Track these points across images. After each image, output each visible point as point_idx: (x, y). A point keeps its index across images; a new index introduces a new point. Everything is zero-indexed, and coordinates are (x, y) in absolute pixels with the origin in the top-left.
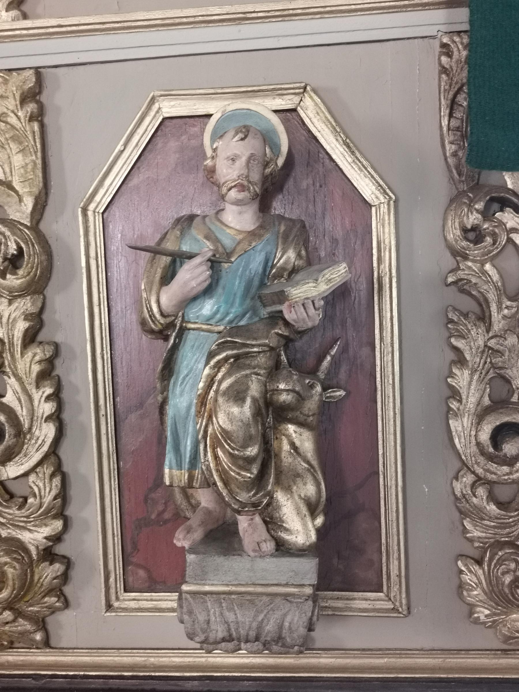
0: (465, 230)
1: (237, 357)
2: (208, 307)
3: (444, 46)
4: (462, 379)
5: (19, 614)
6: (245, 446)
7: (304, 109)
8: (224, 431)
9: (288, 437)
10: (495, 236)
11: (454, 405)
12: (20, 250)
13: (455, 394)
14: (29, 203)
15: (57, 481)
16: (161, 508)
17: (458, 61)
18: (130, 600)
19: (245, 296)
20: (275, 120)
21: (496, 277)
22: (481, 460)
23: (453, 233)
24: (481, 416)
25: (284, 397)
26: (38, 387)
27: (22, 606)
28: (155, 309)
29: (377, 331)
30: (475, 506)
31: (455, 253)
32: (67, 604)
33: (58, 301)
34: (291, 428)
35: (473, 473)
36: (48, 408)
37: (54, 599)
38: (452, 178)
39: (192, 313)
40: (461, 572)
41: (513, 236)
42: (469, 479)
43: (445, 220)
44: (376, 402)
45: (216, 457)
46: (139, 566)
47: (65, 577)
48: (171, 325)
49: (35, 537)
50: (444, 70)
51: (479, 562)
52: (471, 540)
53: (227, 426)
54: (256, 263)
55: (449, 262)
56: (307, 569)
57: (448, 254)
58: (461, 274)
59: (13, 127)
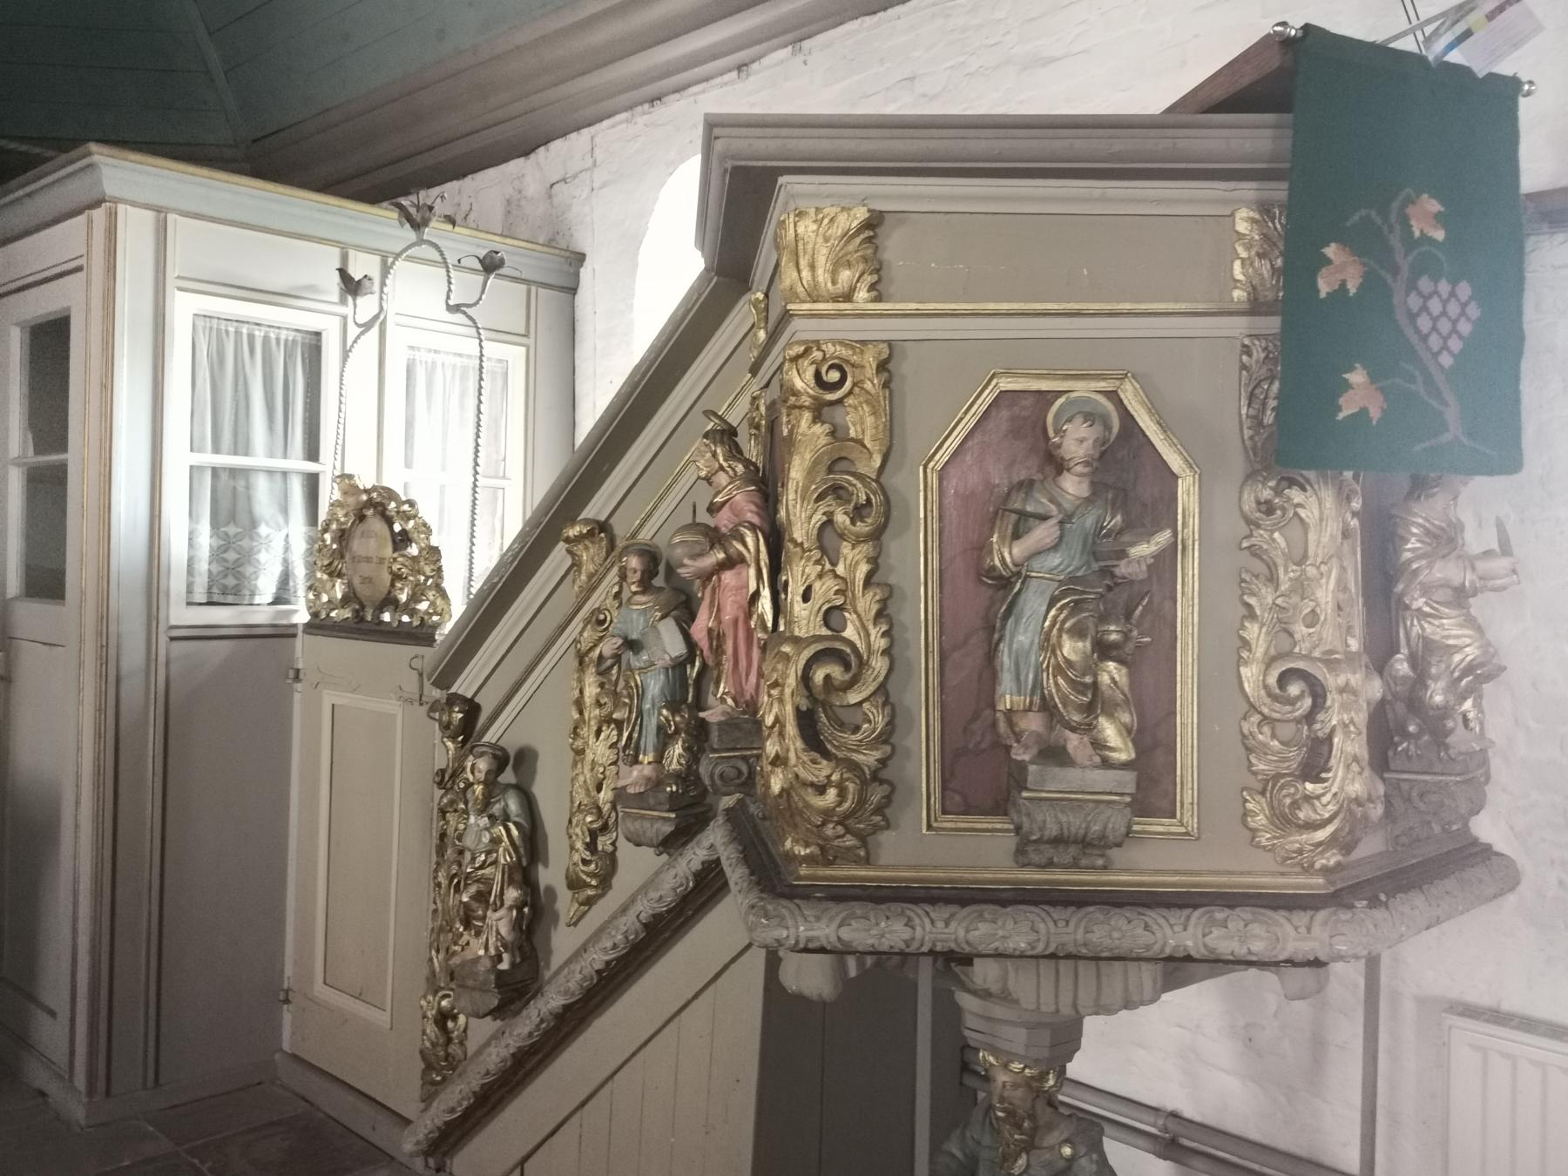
0: (1259, 503)
1: (1076, 602)
2: (1055, 560)
3: (1244, 346)
4: (1252, 631)
5: (848, 831)
6: (1084, 675)
7: (1124, 391)
8: (1067, 661)
9: (1109, 672)
10: (1284, 509)
11: (1245, 654)
12: (868, 500)
13: (1246, 644)
14: (877, 461)
15: (888, 710)
16: (978, 738)
17: (1257, 361)
18: (948, 822)
19: (1082, 553)
20: (1101, 399)
21: (1283, 545)
22: (1268, 701)
23: (1249, 504)
24: (1270, 662)
25: (1114, 637)
26: (875, 624)
27: (850, 822)
28: (1008, 560)
29: (1179, 587)
30: (1261, 743)
31: (1252, 523)
32: (888, 827)
33: (894, 546)
34: (1111, 665)
35: (1260, 713)
36: (881, 643)
37: (879, 818)
38: (1248, 457)
39: (1036, 564)
40: (1246, 801)
41: (1299, 510)
42: (1256, 718)
43: (1241, 493)
44: (1175, 649)
45: (1056, 684)
46: (954, 791)
47: (888, 799)
48: (1019, 574)
49: (868, 758)
50: (1244, 367)
51: (1263, 793)
52: (1255, 774)
53: (1073, 657)
54: (1090, 521)
55: (1243, 529)
56: (1128, 780)
57: (1242, 523)
58: (1253, 541)
59: (868, 392)
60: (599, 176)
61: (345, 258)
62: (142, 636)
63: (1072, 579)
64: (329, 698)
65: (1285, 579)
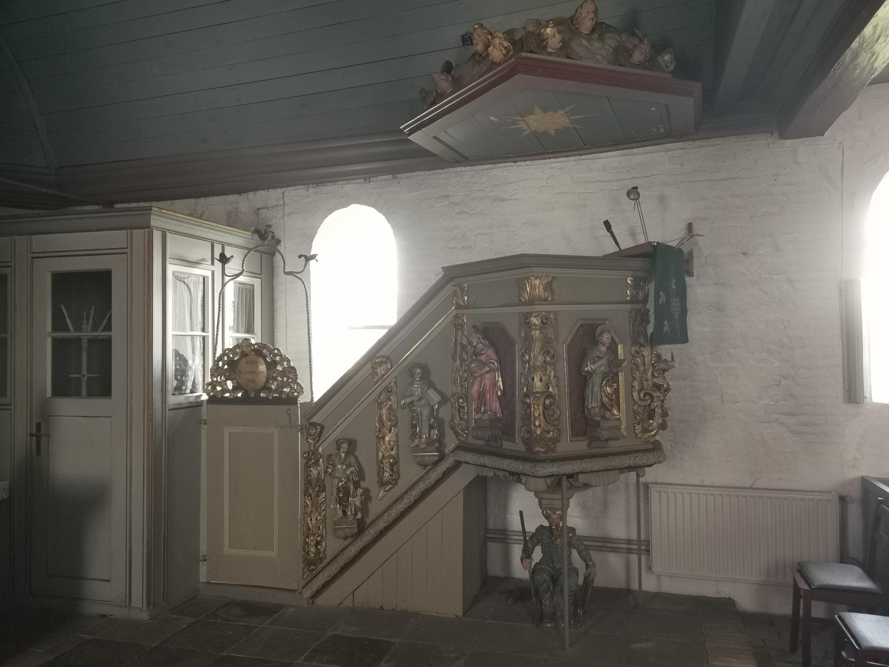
60: (288, 209)
61: (223, 248)
62: (160, 410)
63: (606, 373)
64: (227, 431)
65: (642, 369)
